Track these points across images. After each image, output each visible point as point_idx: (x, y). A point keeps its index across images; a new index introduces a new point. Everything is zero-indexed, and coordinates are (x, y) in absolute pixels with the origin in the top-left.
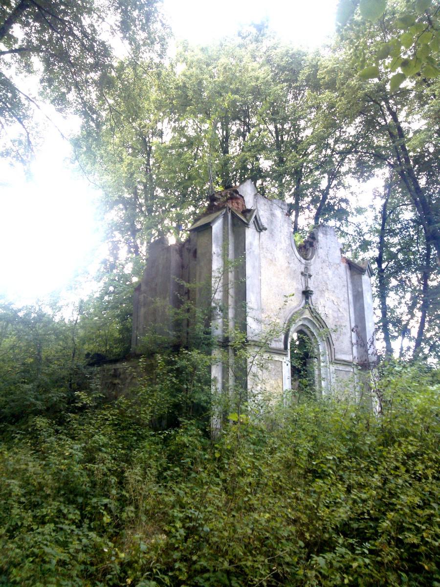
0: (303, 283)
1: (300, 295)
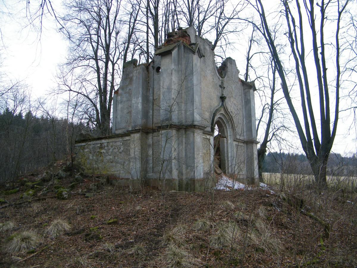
0: (221, 92)
1: (219, 99)
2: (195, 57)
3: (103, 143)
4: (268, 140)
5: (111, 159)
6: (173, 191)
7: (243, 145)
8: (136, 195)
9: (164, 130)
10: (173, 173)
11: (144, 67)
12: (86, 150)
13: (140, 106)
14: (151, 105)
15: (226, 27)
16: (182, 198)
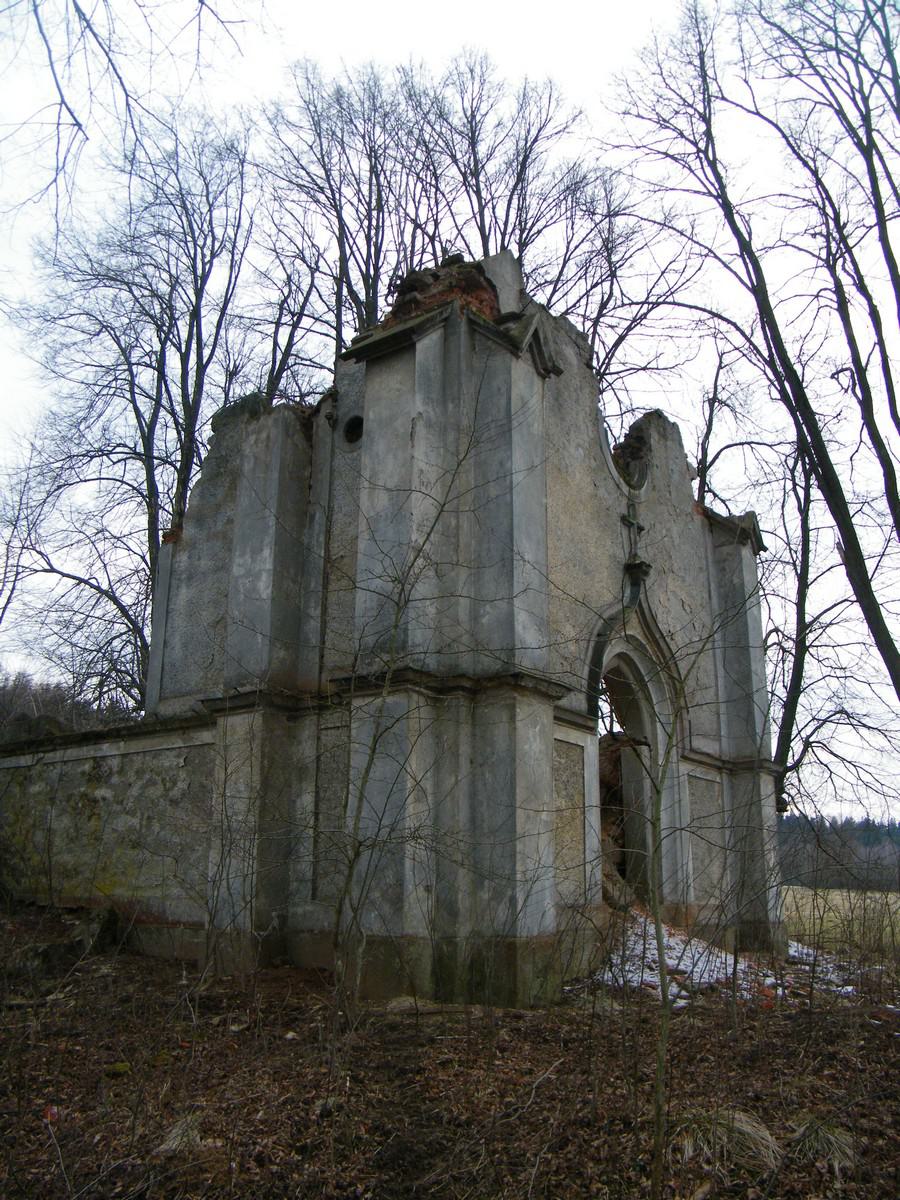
1: (620, 575)
2: (521, 373)
3: (104, 758)
4: (790, 762)
5: (131, 829)
6: (406, 1002)
7: (718, 780)
8: (216, 1020)
9: (364, 696)
10: (406, 908)
11: (293, 417)
12: (35, 789)
13: (264, 587)
14: (315, 584)
15: (619, 353)
16: (450, 1061)
